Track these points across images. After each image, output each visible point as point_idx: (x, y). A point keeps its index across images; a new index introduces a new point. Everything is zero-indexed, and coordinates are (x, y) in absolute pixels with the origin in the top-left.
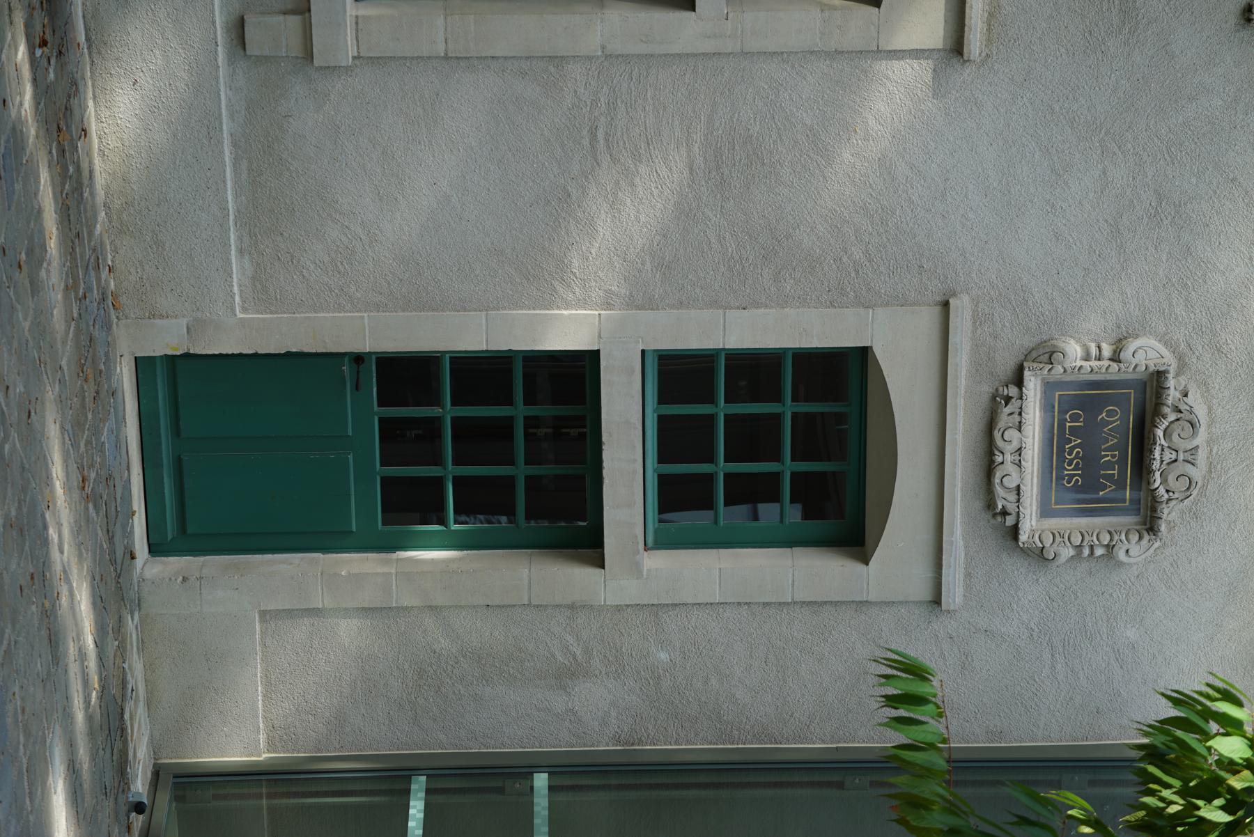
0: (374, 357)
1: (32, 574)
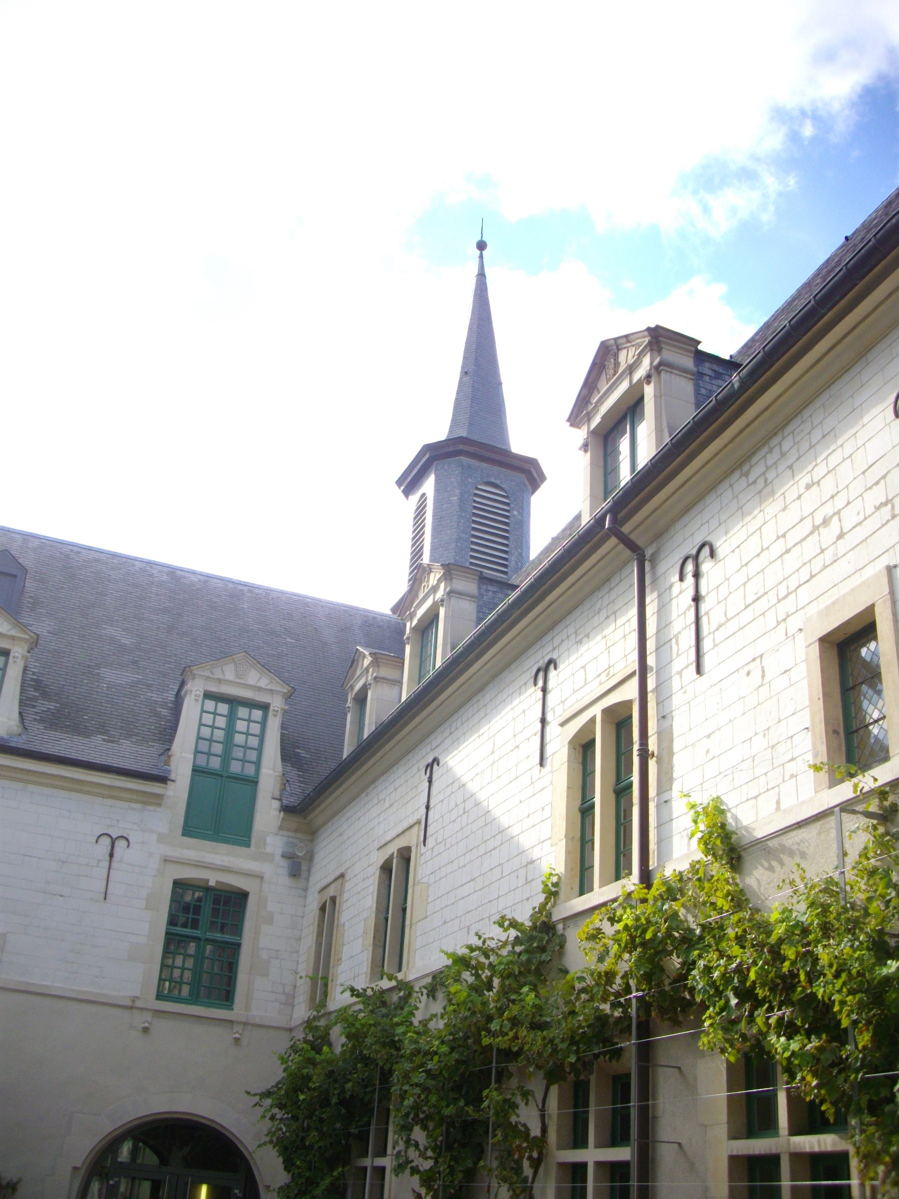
1: (246, 1092)
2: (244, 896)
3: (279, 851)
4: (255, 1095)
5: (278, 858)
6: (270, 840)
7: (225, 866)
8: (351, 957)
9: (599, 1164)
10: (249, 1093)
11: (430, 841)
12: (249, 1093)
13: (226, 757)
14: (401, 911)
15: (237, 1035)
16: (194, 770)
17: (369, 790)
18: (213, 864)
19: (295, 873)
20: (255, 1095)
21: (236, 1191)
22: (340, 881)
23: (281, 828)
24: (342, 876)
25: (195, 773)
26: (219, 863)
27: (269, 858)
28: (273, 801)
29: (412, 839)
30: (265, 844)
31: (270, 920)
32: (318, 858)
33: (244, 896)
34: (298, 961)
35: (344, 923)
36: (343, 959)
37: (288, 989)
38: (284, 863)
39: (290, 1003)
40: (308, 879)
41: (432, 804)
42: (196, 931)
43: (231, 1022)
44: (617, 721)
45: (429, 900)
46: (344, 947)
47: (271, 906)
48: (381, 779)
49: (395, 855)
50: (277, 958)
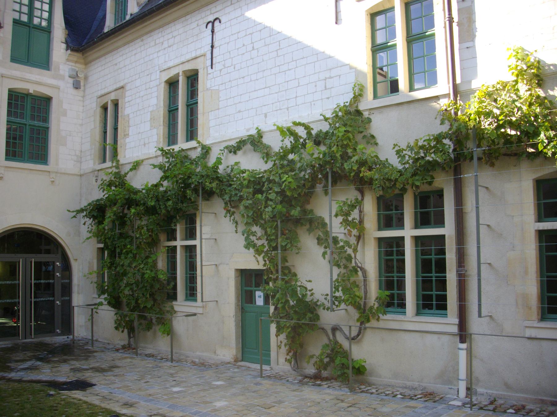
0: (45, 125)
2: (48, 99)
3: (67, 74)
4: (73, 212)
5: (67, 78)
6: (61, 67)
7: (37, 81)
8: (139, 133)
9: (182, 246)
10: (69, 211)
11: (216, 66)
12: (69, 211)
13: (31, 15)
14: (99, 111)
15: (53, 180)
16: (14, 22)
17: (144, 37)
18: (25, 79)
19: (77, 86)
20: (73, 212)
21: (58, 264)
22: (121, 90)
23: (68, 60)
24: (122, 87)
25: (15, 24)
26: (34, 79)
27: (62, 78)
28: (62, 44)
29: (198, 65)
30: (59, 70)
31: (65, 114)
32: (90, 79)
33: (48, 99)
34: (82, 137)
35: (129, 115)
36: (130, 135)
37: (78, 153)
38: (71, 81)
39: (79, 160)
40: (84, 91)
41: (216, 44)
42: (23, 120)
43: (49, 172)
44: (406, 1)
45: (220, 99)
46: (131, 128)
47: (65, 106)
48: (157, 31)
49: (180, 74)
50: (70, 136)
